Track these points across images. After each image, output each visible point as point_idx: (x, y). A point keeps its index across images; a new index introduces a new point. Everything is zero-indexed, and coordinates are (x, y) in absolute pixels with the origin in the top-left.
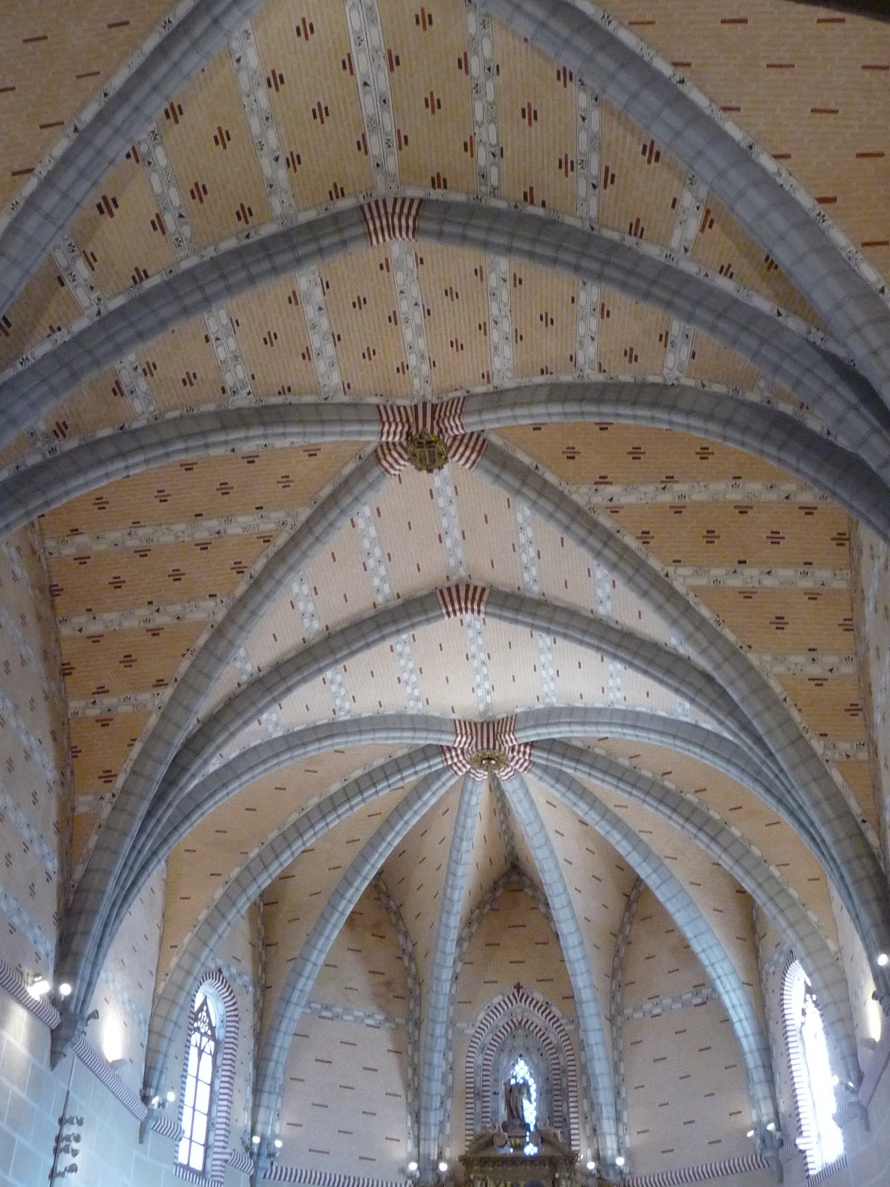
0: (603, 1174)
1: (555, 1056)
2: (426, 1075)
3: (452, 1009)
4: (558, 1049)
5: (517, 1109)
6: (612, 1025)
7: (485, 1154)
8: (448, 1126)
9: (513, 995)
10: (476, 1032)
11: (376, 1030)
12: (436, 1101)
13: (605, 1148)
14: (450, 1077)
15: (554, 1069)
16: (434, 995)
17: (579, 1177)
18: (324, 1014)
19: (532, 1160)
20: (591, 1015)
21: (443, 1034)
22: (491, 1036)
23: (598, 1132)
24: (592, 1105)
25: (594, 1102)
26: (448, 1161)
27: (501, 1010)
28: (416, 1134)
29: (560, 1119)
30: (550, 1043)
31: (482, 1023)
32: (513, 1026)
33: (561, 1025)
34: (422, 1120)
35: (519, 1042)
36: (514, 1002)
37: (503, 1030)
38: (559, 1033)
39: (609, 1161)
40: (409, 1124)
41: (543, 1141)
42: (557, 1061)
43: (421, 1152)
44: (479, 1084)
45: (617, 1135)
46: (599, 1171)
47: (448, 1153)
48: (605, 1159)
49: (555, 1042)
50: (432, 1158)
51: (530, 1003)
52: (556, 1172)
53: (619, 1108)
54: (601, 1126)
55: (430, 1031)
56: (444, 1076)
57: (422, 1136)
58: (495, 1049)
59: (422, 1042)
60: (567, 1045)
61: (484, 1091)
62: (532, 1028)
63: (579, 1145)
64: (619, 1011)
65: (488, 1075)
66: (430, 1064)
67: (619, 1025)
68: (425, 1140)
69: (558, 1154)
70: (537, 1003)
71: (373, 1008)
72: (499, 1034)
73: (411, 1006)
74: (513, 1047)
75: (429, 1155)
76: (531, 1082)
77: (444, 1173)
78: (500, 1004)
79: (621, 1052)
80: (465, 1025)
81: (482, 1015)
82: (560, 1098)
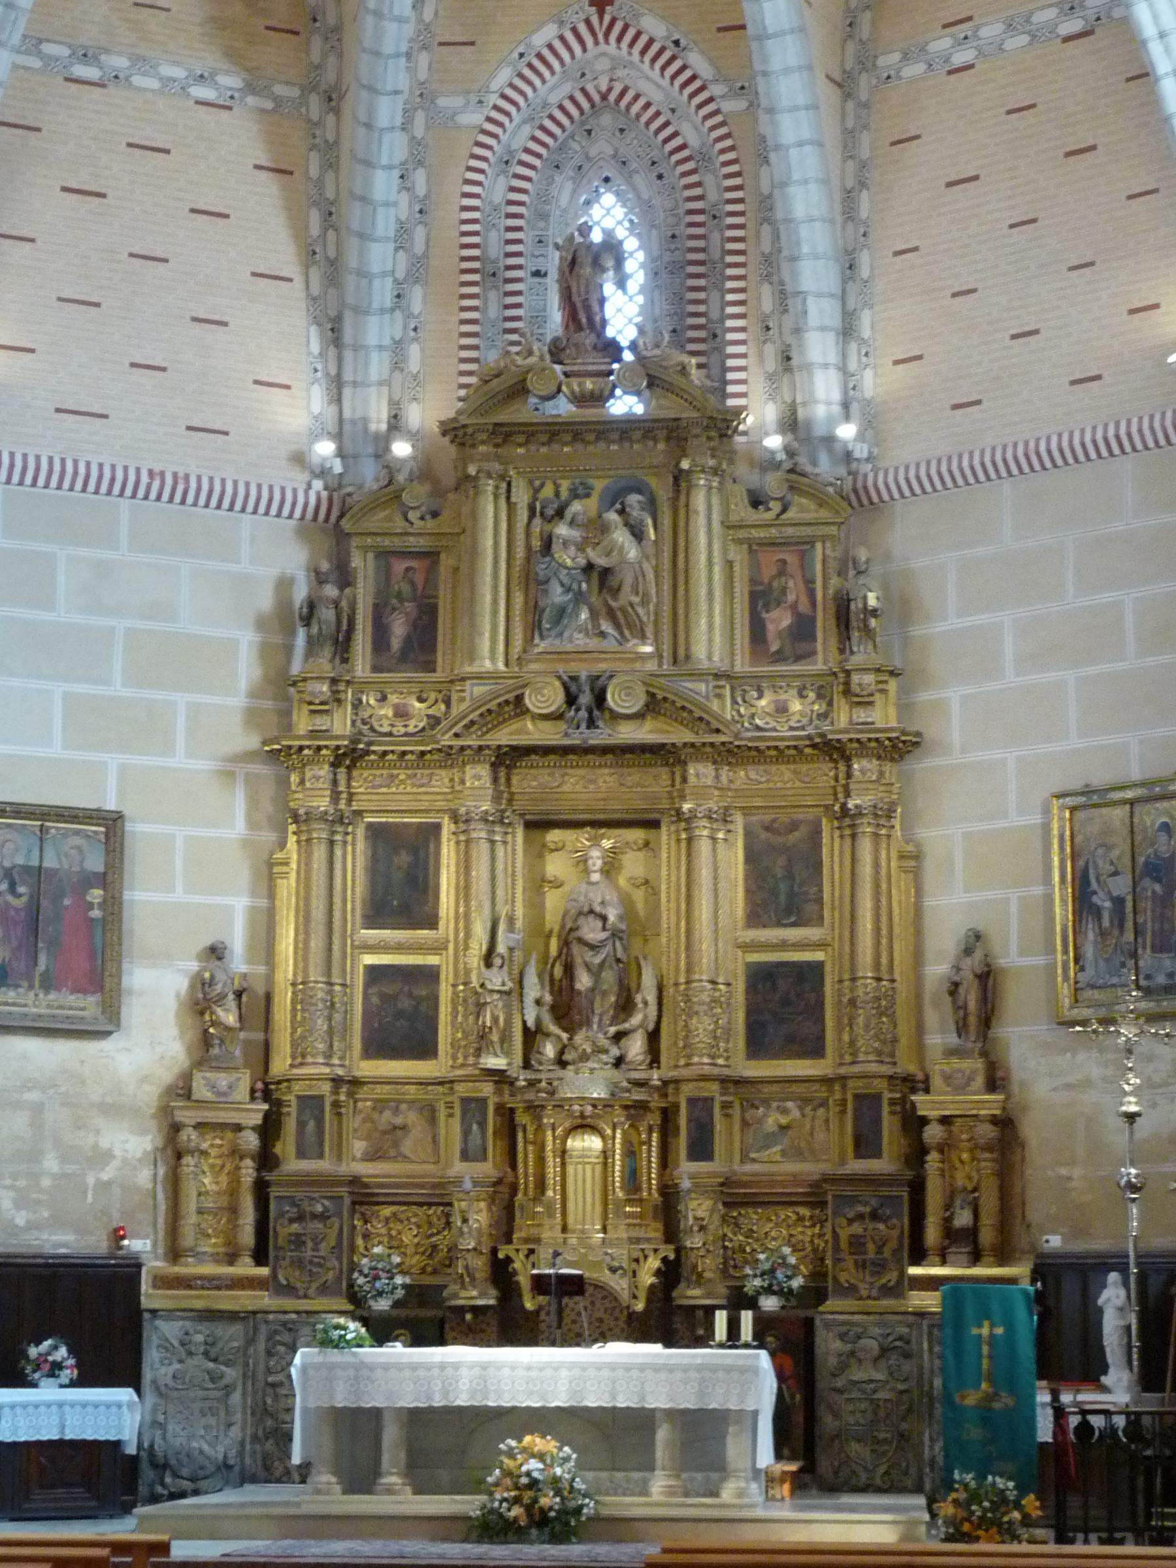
0: (803, 461)
1: (694, 179)
2: (355, 225)
3: (423, 59)
4: (702, 158)
5: (588, 308)
6: (847, 95)
7: (504, 416)
8: (414, 351)
9: (588, 22)
10: (489, 119)
11: (224, 114)
12: (383, 292)
13: (811, 401)
14: (420, 233)
15: (691, 212)
16: (370, 20)
17: (741, 469)
18: (80, 71)
19: (626, 428)
20: (787, 71)
21: (399, 121)
22: (527, 130)
23: (794, 362)
24: (784, 298)
25: (789, 288)
26: (414, 437)
27: (556, 64)
28: (333, 372)
29: (702, 334)
30: (683, 147)
31: (504, 97)
32: (585, 105)
33: (711, 100)
34: (348, 336)
35: (602, 147)
36: (589, 41)
37: (558, 115)
38: (706, 118)
39: (819, 431)
40: (315, 347)
41: (653, 382)
42: (697, 191)
43: (347, 414)
44: (495, 248)
45: (843, 369)
46: (790, 452)
47: (416, 416)
48: (809, 424)
49: (693, 140)
50: (373, 427)
51: (631, 45)
52: (684, 455)
53: (851, 304)
54: (801, 346)
55: (363, 118)
56: (403, 233)
57: (348, 376)
58: (537, 162)
59: (345, 146)
60: (723, 151)
61: (509, 268)
62: (635, 109)
63: (743, 395)
64: (866, 63)
65: (519, 229)
66: (364, 199)
67: (864, 97)
68: (355, 384)
69: (688, 414)
70: (651, 41)
71: (209, 58)
72: (548, 124)
73: (316, 58)
74: (588, 158)
75: (365, 420)
76: (631, 244)
77: (403, 461)
78: (550, 47)
79: (863, 165)
80: (458, 102)
81: (505, 75)
82: (702, 282)
